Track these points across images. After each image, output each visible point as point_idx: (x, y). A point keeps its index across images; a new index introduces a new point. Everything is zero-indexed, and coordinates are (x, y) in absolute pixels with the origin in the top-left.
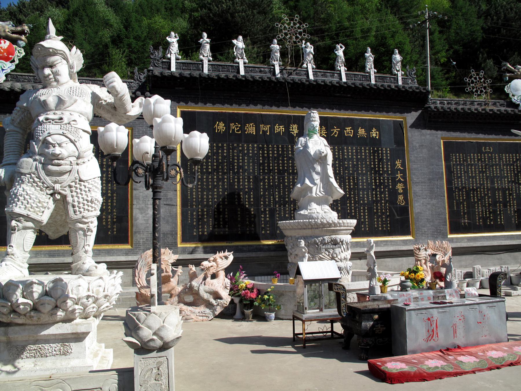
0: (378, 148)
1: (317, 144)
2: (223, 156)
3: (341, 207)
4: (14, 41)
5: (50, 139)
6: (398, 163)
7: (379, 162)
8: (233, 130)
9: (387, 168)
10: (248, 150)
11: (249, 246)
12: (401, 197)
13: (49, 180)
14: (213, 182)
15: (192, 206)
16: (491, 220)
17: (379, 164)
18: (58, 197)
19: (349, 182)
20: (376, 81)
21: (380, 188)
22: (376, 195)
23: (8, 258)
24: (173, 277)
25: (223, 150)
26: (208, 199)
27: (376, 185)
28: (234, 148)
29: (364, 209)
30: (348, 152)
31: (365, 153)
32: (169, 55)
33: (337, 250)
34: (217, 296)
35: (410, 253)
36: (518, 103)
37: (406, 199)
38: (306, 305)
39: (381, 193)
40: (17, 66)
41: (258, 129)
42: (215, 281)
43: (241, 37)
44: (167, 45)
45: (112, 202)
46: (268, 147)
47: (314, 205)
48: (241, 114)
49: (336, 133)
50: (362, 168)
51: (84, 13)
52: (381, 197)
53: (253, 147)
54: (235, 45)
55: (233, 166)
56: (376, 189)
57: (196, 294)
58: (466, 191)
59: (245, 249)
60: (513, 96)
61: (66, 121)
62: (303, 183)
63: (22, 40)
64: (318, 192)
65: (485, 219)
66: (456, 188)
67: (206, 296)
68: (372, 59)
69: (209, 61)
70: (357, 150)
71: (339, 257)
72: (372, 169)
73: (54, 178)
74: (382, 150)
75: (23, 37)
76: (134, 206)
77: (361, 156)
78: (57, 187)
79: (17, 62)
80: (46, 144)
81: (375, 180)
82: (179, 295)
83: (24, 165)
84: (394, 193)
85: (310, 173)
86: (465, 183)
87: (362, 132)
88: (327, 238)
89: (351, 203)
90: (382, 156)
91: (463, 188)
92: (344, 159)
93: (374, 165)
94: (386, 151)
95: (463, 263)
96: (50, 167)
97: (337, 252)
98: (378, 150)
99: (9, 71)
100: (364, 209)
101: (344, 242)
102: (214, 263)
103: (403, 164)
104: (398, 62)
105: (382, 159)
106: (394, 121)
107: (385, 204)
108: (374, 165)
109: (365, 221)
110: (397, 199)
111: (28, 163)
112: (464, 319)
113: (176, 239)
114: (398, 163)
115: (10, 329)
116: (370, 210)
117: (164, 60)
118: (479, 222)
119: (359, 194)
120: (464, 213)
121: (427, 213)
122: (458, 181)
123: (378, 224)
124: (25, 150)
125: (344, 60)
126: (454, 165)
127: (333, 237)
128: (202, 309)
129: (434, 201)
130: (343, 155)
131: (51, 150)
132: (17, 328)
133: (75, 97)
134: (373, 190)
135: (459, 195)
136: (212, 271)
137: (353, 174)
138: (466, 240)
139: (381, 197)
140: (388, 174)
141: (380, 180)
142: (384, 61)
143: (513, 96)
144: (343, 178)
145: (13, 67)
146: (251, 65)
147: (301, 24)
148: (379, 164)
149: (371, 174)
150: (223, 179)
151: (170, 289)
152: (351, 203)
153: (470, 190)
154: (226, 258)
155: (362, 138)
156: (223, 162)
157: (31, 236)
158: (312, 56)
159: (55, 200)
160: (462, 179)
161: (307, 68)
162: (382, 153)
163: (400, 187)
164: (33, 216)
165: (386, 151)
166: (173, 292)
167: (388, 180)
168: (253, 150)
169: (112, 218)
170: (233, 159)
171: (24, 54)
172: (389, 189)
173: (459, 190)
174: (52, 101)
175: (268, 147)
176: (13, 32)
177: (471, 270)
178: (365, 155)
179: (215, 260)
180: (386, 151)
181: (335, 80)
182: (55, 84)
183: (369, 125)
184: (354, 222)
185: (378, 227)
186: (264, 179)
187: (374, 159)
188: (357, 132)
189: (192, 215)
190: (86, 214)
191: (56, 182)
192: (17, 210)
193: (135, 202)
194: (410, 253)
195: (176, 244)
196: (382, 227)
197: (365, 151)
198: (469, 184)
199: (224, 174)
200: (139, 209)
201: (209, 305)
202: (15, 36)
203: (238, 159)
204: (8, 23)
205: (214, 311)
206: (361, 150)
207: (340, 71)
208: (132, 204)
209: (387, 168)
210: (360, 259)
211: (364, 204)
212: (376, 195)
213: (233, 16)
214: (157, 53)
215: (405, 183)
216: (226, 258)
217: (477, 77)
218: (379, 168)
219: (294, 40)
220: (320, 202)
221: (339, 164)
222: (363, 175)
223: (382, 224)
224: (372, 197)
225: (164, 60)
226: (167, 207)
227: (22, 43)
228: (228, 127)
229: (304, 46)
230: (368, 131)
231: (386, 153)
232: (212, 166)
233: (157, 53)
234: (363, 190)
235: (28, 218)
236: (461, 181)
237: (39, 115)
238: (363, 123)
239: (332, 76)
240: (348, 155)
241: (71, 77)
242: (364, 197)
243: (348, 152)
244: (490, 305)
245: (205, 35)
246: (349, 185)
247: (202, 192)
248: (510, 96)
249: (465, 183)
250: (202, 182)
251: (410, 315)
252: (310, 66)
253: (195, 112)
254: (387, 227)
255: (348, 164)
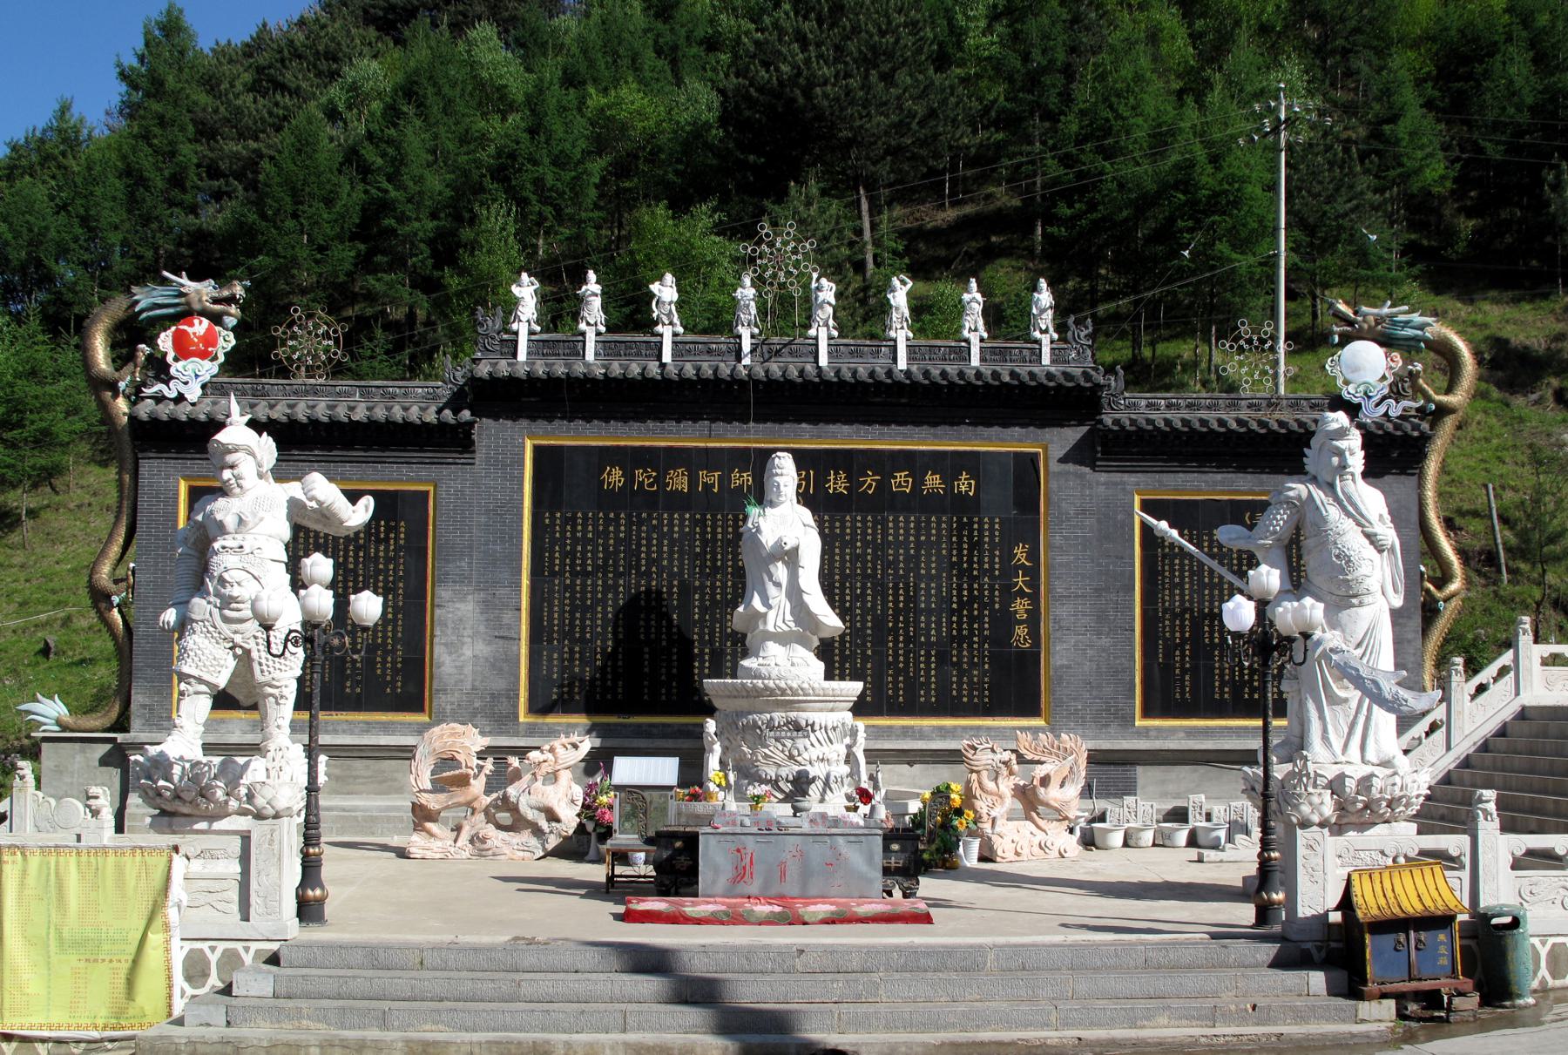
0: (970, 519)
1: (786, 523)
2: (617, 539)
3: (835, 657)
4: (216, 319)
5: (226, 576)
6: (1020, 553)
7: (971, 551)
8: (641, 484)
9: (992, 563)
10: (671, 525)
11: (664, 725)
12: (1021, 631)
13: (226, 629)
14: (594, 592)
15: (550, 641)
16: (1253, 690)
17: (971, 556)
18: (239, 651)
19: (896, 595)
20: (983, 360)
21: (971, 610)
22: (960, 623)
23: (175, 732)
24: (476, 777)
25: (618, 526)
26: (583, 627)
27: (960, 602)
28: (640, 522)
29: (928, 655)
30: (896, 528)
31: (939, 529)
32: (515, 326)
33: (801, 743)
34: (552, 817)
35: (954, 757)
36: (1356, 401)
37: (1034, 633)
38: (616, 826)
39: (972, 619)
40: (221, 366)
41: (693, 482)
42: (550, 788)
43: (669, 278)
44: (512, 305)
45: (394, 631)
46: (714, 520)
47: (772, 648)
48: (659, 448)
49: (870, 486)
50: (928, 563)
51: (430, 91)
52: (971, 630)
53: (682, 520)
54: (654, 295)
55: (639, 560)
56: (960, 610)
57: (514, 809)
58: (1192, 618)
59: (655, 731)
60: (1347, 383)
61: (247, 549)
62: (749, 604)
63: (230, 315)
64: (779, 623)
65: (1237, 688)
66: (1165, 611)
67: (531, 815)
68: (978, 308)
69: (598, 334)
70: (918, 522)
71: (805, 755)
72: (952, 565)
73: (235, 627)
74: (980, 523)
75: (233, 309)
76: (436, 640)
77: (929, 535)
78: (238, 639)
79: (222, 359)
80: (222, 581)
81: (960, 589)
82: (486, 811)
83: (196, 609)
84: (1005, 621)
85: (763, 584)
86: (1191, 601)
87: (933, 481)
88: (778, 716)
89: (896, 641)
90: (981, 536)
91: (1184, 611)
92: (886, 544)
93: (960, 555)
94: (990, 525)
95: (1171, 788)
96: (227, 612)
97: (801, 748)
98: (971, 523)
99: (207, 378)
100: (928, 655)
101: (817, 727)
102: (550, 756)
103: (1033, 555)
104: (1043, 311)
105: (980, 543)
106: (1016, 454)
107: (981, 644)
108: (960, 555)
109: (928, 683)
110: (1011, 633)
111: (200, 607)
112: (802, 855)
113: (516, 706)
114: (1020, 553)
115: (176, 820)
116: (943, 658)
117: (505, 337)
118: (1222, 693)
119: (917, 622)
120: (1184, 671)
121: (1086, 668)
122: (1172, 595)
123: (960, 690)
124: (199, 588)
125: (907, 314)
126: (1164, 556)
127: (793, 715)
128: (526, 837)
129: (1105, 641)
130: (885, 534)
131: (227, 591)
132: (182, 820)
133: (261, 514)
134: (953, 612)
135: (1173, 626)
136: (545, 768)
137: (906, 576)
138: (1182, 735)
139: (971, 630)
140: (992, 577)
141: (970, 590)
142: (1181, 231)
143: (1347, 383)
144: (882, 585)
145: (216, 370)
146: (690, 338)
147: (799, 241)
148: (971, 556)
149: (950, 578)
150: (616, 586)
151: (469, 798)
152: (896, 641)
153: (1205, 616)
154: (575, 746)
155: (933, 495)
156: (616, 552)
157: (206, 703)
158: (830, 310)
159: (235, 656)
160: (1182, 590)
161: (816, 338)
162: (981, 530)
163: (1020, 607)
164: (206, 677)
165: (992, 524)
166: (475, 805)
167: (992, 589)
168: (682, 525)
169: (394, 663)
170: (639, 545)
171: (234, 342)
172: (992, 610)
173: (1175, 616)
174: (230, 522)
175: (714, 520)
176: (216, 301)
177: (1180, 803)
178: (939, 535)
179: (552, 750)
180: (992, 524)
181: (880, 366)
182: (237, 490)
183: (950, 465)
184: (857, 687)
185: (960, 696)
186: (703, 587)
187: (960, 542)
188: (923, 482)
189: (550, 659)
190: (277, 674)
191: (236, 632)
192: (186, 669)
193: (437, 632)
194: (954, 757)
195: (517, 717)
196: (971, 696)
197: (940, 525)
198: (1201, 602)
199: (618, 575)
200: (446, 645)
201: (538, 832)
202: (218, 307)
203: (649, 546)
204: (206, 283)
205: (544, 843)
206: (928, 522)
207: (895, 340)
208: (432, 636)
209: (992, 563)
210: (911, 764)
211: (929, 644)
212: (960, 623)
213: (807, 92)
214: (490, 323)
215: (1034, 598)
216: (575, 746)
217: (1255, 338)
218: (970, 562)
219: (782, 280)
220: (783, 639)
221: (874, 553)
222: (930, 578)
223: (971, 690)
224: (950, 629)
225: (505, 337)
226: (501, 642)
227: (231, 321)
228: (629, 477)
229: (814, 285)
230: (950, 478)
231: (992, 529)
232: (594, 559)
233: (490, 323)
234: (929, 612)
235: (200, 680)
236: (1182, 595)
237: (215, 540)
238: (937, 461)
239: (876, 354)
240: (896, 535)
241: (261, 476)
242: (928, 629)
243: (896, 528)
244: (852, 839)
245: (592, 275)
246: (896, 602)
247: (572, 613)
248: (1340, 382)
249: (1191, 601)
250: (573, 592)
251: (707, 842)
252: (822, 332)
253: (561, 447)
254: (981, 697)
255: (896, 555)
